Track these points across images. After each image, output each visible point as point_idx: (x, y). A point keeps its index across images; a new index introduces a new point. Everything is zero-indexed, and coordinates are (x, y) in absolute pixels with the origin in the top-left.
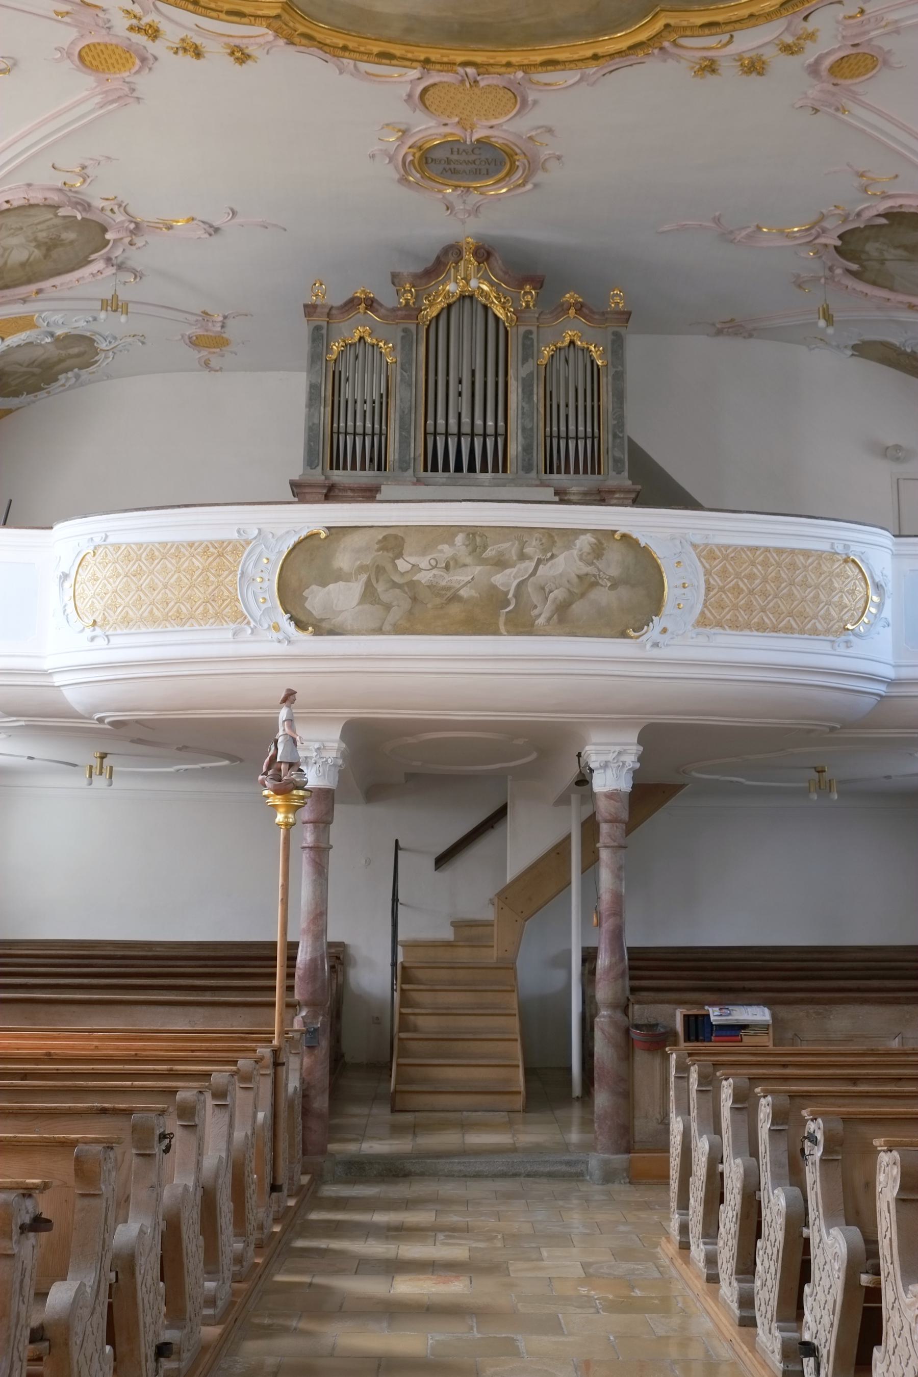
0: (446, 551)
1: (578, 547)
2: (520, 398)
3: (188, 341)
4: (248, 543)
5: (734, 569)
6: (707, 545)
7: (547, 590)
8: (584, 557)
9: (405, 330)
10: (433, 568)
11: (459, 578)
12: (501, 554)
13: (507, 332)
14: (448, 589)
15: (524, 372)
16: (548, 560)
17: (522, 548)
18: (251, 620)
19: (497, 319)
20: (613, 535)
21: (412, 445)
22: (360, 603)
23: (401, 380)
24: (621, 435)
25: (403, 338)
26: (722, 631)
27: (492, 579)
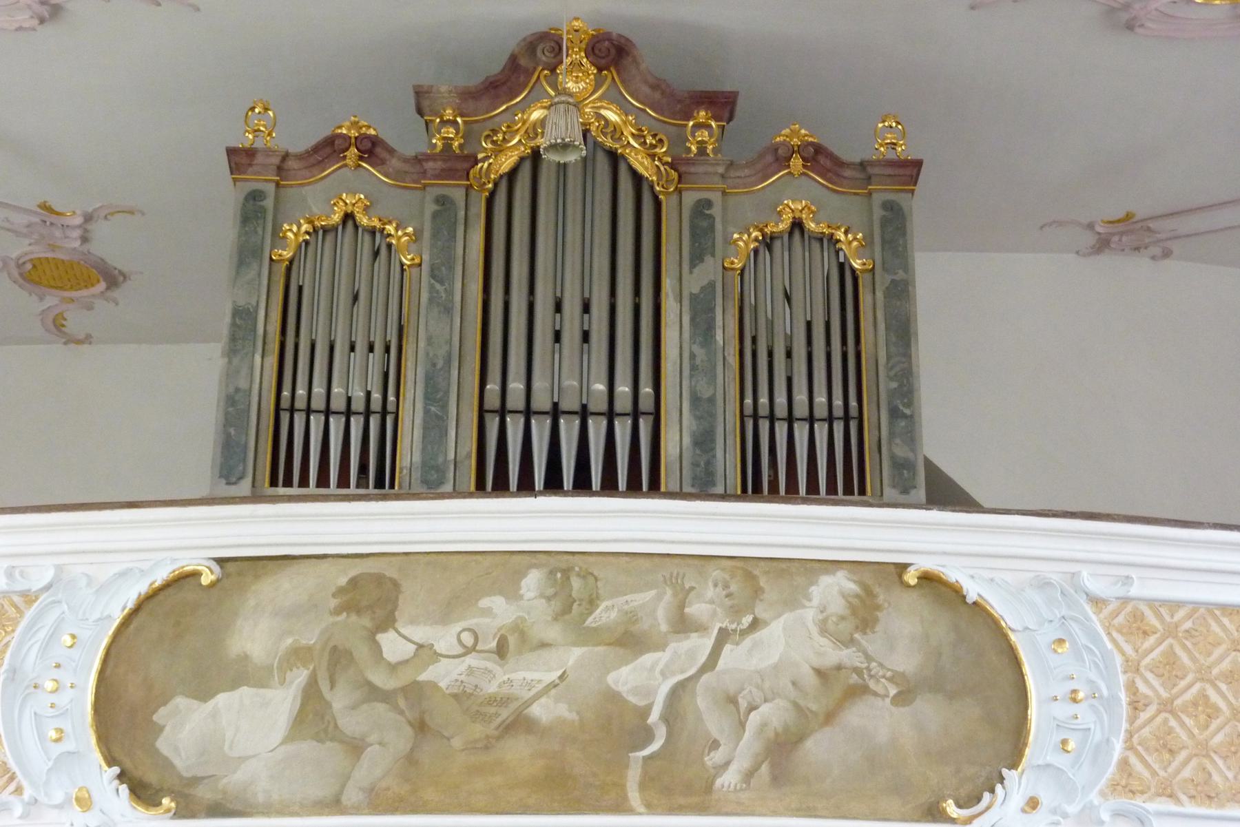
0: (498, 611)
1: (815, 602)
2: (686, 335)
3: (15, 273)
4: (29, 598)
5: (1194, 659)
6: (1126, 600)
7: (743, 704)
8: (830, 626)
9: (442, 201)
10: (468, 651)
11: (529, 675)
12: (631, 617)
13: (658, 204)
14: (504, 701)
15: (695, 282)
16: (744, 633)
17: (682, 606)
18: (25, 784)
19: (637, 178)
20: (900, 576)
21: (452, 433)
22: (288, 739)
23: (431, 300)
24: (907, 412)
25: (435, 216)
26: (1173, 808)
27: (611, 679)
